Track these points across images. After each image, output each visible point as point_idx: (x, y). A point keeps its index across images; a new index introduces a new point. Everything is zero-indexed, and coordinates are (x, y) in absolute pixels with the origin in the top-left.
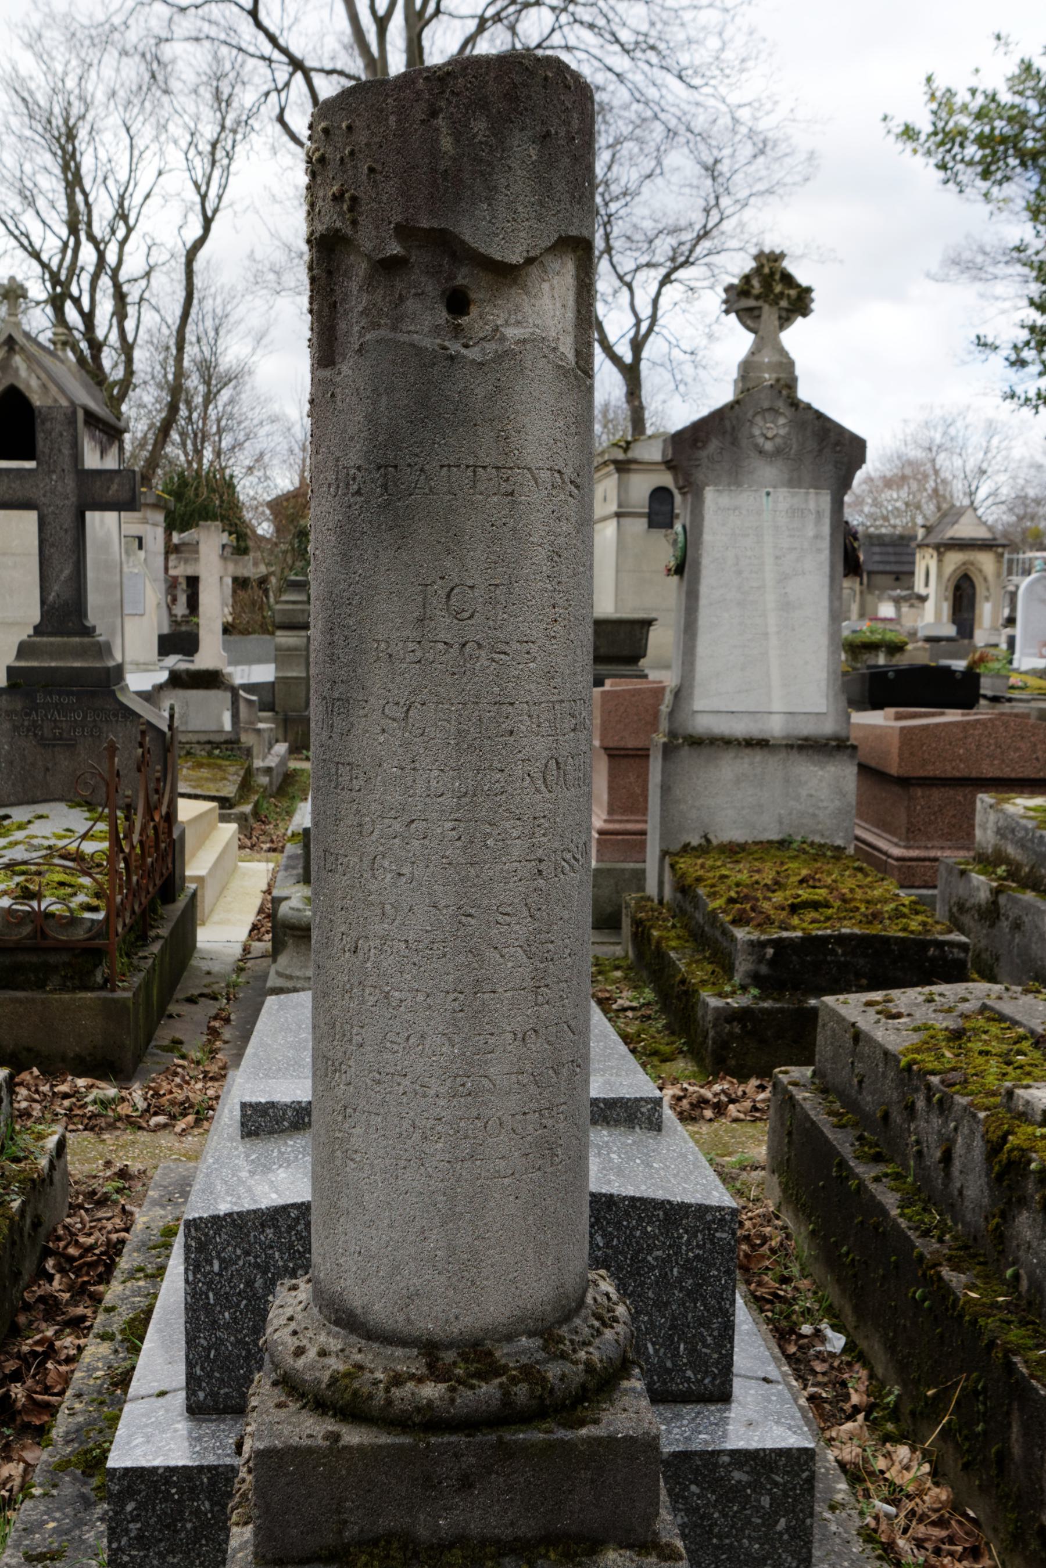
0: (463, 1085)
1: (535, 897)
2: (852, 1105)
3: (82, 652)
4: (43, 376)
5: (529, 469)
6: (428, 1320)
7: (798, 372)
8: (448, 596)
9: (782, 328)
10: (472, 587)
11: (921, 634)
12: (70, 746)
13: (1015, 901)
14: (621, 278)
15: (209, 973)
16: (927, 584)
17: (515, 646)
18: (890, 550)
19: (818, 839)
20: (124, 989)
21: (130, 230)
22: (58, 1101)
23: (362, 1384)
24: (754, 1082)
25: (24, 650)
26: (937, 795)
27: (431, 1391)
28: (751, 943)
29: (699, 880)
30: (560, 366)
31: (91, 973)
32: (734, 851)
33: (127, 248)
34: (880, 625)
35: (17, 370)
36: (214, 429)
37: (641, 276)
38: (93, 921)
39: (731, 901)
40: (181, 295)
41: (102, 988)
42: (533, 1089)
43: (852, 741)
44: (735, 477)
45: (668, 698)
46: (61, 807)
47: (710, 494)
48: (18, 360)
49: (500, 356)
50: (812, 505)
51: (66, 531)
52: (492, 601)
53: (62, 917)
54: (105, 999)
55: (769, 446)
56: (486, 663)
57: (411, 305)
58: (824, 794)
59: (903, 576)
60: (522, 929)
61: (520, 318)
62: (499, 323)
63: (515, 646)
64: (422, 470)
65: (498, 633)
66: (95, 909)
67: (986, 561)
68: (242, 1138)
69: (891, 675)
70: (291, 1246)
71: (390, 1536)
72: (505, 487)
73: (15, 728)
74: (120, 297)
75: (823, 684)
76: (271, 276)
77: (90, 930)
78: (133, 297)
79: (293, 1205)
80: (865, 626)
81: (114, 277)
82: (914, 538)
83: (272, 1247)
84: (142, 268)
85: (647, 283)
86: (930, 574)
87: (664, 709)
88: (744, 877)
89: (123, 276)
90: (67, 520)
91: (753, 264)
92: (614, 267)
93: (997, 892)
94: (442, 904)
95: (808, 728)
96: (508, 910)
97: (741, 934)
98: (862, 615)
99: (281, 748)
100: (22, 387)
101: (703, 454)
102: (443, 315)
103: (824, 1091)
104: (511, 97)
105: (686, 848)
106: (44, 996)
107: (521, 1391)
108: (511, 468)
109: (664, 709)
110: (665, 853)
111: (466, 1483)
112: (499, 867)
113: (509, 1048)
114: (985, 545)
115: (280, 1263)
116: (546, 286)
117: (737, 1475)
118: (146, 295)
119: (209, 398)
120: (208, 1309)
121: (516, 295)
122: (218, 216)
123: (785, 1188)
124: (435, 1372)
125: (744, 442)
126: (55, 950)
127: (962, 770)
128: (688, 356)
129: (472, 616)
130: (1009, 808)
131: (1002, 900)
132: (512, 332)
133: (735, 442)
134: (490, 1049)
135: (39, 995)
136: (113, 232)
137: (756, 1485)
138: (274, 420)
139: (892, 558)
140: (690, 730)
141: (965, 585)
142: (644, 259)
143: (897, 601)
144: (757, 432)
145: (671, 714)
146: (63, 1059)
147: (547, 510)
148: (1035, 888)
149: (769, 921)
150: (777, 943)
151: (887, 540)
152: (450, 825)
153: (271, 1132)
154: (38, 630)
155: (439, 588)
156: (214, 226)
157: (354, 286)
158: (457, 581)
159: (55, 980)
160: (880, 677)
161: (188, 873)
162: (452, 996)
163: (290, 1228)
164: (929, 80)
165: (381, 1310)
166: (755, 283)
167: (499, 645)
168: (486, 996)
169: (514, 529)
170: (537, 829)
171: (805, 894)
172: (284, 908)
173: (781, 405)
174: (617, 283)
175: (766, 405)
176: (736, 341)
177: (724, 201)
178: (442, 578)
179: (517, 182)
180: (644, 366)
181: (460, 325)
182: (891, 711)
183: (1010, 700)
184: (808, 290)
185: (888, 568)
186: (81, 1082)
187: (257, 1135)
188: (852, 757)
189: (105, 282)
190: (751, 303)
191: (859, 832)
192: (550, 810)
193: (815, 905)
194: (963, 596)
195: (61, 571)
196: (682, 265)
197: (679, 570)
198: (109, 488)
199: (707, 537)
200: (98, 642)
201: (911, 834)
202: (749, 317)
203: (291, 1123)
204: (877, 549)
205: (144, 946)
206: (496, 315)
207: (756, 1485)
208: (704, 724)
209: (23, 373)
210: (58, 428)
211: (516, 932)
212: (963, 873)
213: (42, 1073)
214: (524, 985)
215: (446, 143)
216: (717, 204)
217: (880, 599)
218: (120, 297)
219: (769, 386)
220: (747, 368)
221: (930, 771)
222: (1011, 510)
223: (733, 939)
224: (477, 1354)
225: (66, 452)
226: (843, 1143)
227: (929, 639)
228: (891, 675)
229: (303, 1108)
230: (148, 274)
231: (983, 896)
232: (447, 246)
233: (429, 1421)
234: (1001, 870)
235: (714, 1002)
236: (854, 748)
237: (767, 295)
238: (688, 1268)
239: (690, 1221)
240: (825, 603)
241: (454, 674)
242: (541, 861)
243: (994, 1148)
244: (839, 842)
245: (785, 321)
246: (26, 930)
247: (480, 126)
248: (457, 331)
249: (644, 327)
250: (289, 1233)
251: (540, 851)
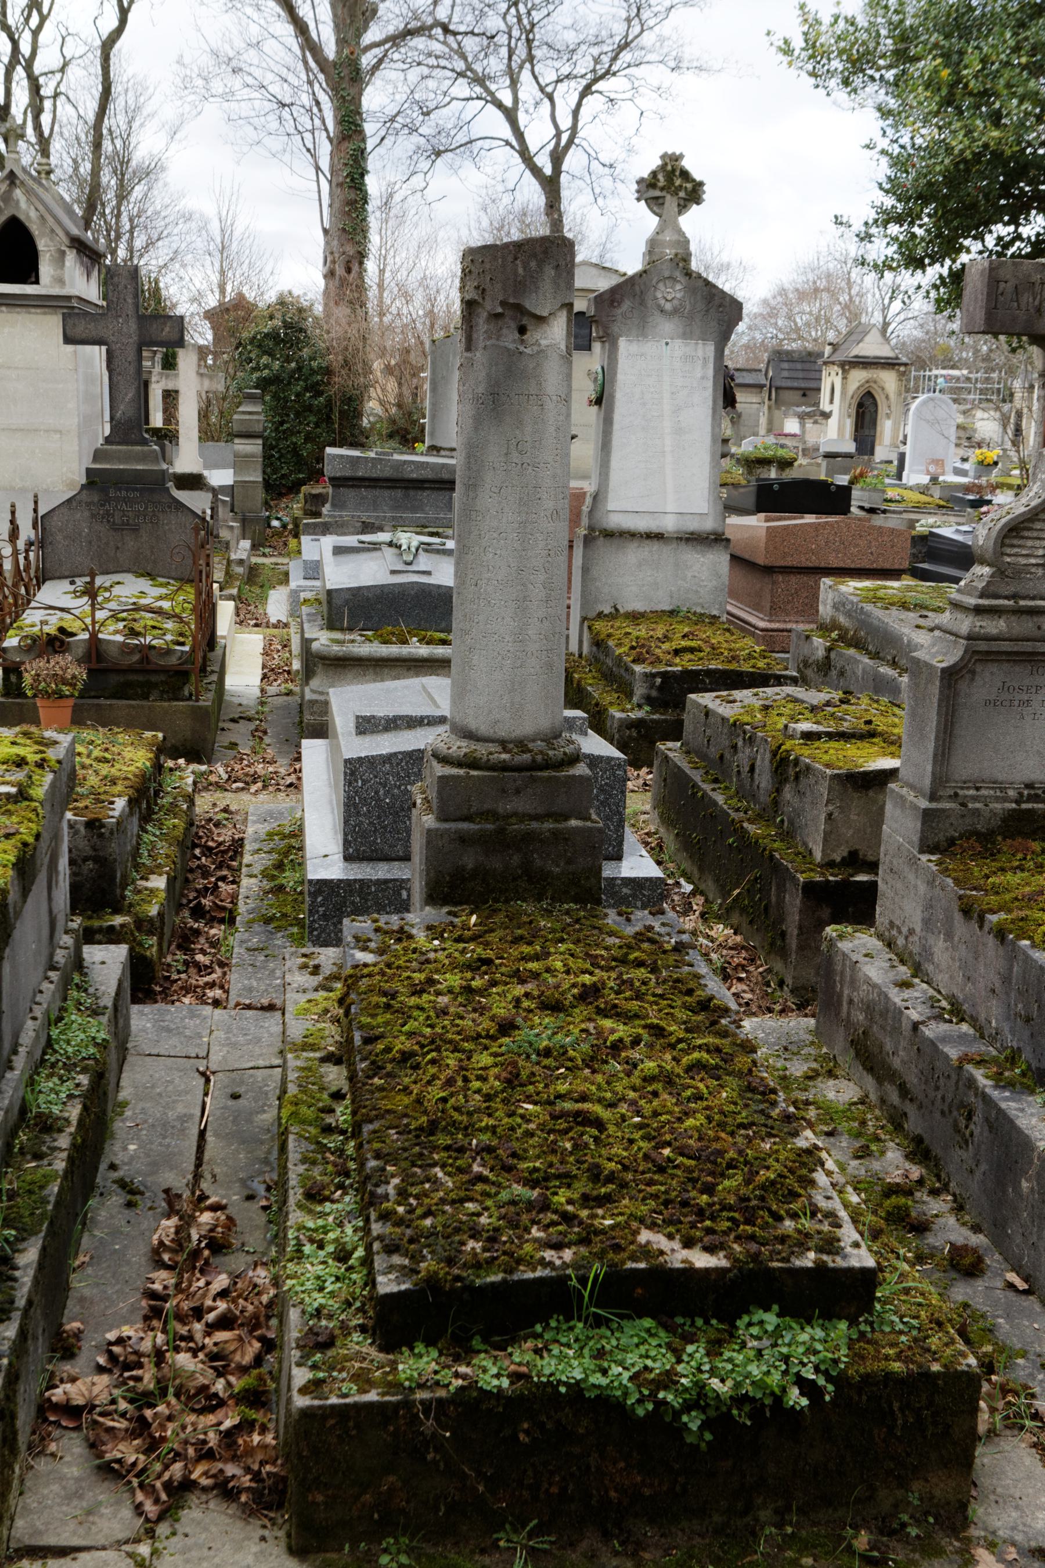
2: (704, 757)
4: (41, 207)
6: (502, 733)
7: (693, 248)
9: (680, 213)
11: (823, 449)
12: (135, 530)
13: (841, 655)
14: (542, 89)
16: (831, 402)
18: (799, 366)
19: (699, 610)
21: (43, 19)
23: (478, 755)
24: (645, 770)
25: (97, 456)
26: (794, 580)
27: (505, 756)
28: (646, 675)
29: (609, 636)
31: (181, 688)
32: (635, 617)
33: (42, 38)
34: (787, 442)
36: (127, 227)
37: (562, 87)
39: (633, 648)
40: (97, 90)
41: (189, 699)
43: (727, 535)
44: (643, 330)
45: (588, 500)
46: (128, 578)
47: (622, 343)
48: (18, 193)
50: (700, 353)
55: (668, 306)
57: (505, 331)
58: (705, 576)
59: (809, 392)
60: (542, 577)
66: (183, 644)
67: (889, 380)
69: (776, 487)
71: (488, 811)
73: (93, 516)
74: (35, 88)
75: (706, 492)
76: (200, 82)
78: (47, 91)
80: (771, 440)
81: (29, 68)
82: (821, 355)
84: (58, 63)
85: (567, 96)
86: (836, 391)
87: (585, 509)
88: (643, 633)
89: (38, 68)
91: (659, 162)
92: (536, 78)
93: (829, 650)
95: (693, 525)
97: (638, 668)
98: (769, 430)
99: (246, 544)
100: (22, 217)
101: (619, 311)
102: (517, 335)
103: (688, 752)
104: (545, 252)
105: (600, 615)
107: (539, 758)
109: (585, 509)
110: (584, 619)
111: (518, 792)
114: (889, 364)
117: (625, 890)
118: (62, 88)
119: (122, 195)
120: (355, 805)
121: (545, 327)
122: (134, 7)
123: (661, 816)
124: (505, 750)
125: (650, 303)
126: (155, 672)
127: (814, 562)
128: (607, 170)
130: (843, 588)
131: (833, 655)
132: (543, 342)
133: (642, 303)
135: (145, 703)
136: (27, 20)
137: (634, 896)
138: (188, 217)
139: (800, 375)
140: (605, 526)
141: (868, 402)
142: (565, 70)
143: (802, 417)
144: (659, 295)
145: (591, 512)
148: (856, 647)
149: (659, 660)
150: (664, 675)
151: (796, 356)
154: (108, 440)
156: (130, 16)
157: (481, 321)
160: (781, 491)
164: (802, 7)
165: (484, 729)
166: (661, 177)
171: (684, 643)
172: (315, 646)
173: (678, 274)
174: (540, 95)
175: (667, 274)
176: (646, 221)
177: (645, 14)
179: (546, 285)
180: (564, 178)
182: (762, 515)
183: (884, 512)
184: (701, 184)
185: (795, 384)
188: (726, 547)
189: (20, 72)
190: (657, 193)
191: (729, 608)
193: (692, 650)
194: (865, 413)
196: (602, 77)
197: (599, 401)
199: (620, 377)
201: (774, 611)
202: (655, 203)
204: (785, 365)
206: (537, 335)
207: (634, 896)
208: (616, 521)
209: (23, 204)
210: (124, 282)
212: (808, 637)
215: (521, 271)
216: (638, 15)
217: (786, 415)
218: (35, 88)
219: (671, 261)
220: (653, 245)
221: (789, 562)
222: (921, 326)
223: (633, 673)
224: (521, 745)
226: (697, 776)
227: (829, 456)
228: (776, 487)
230: (62, 70)
231: (821, 653)
232: (519, 309)
233: (504, 767)
234: (834, 635)
235: (618, 715)
236: (728, 540)
237: (669, 187)
238: (601, 790)
239: (603, 765)
240: (709, 429)
243: (774, 753)
244: (715, 612)
245: (683, 208)
246: (136, 657)
247: (533, 264)
248: (522, 341)
249: (565, 138)
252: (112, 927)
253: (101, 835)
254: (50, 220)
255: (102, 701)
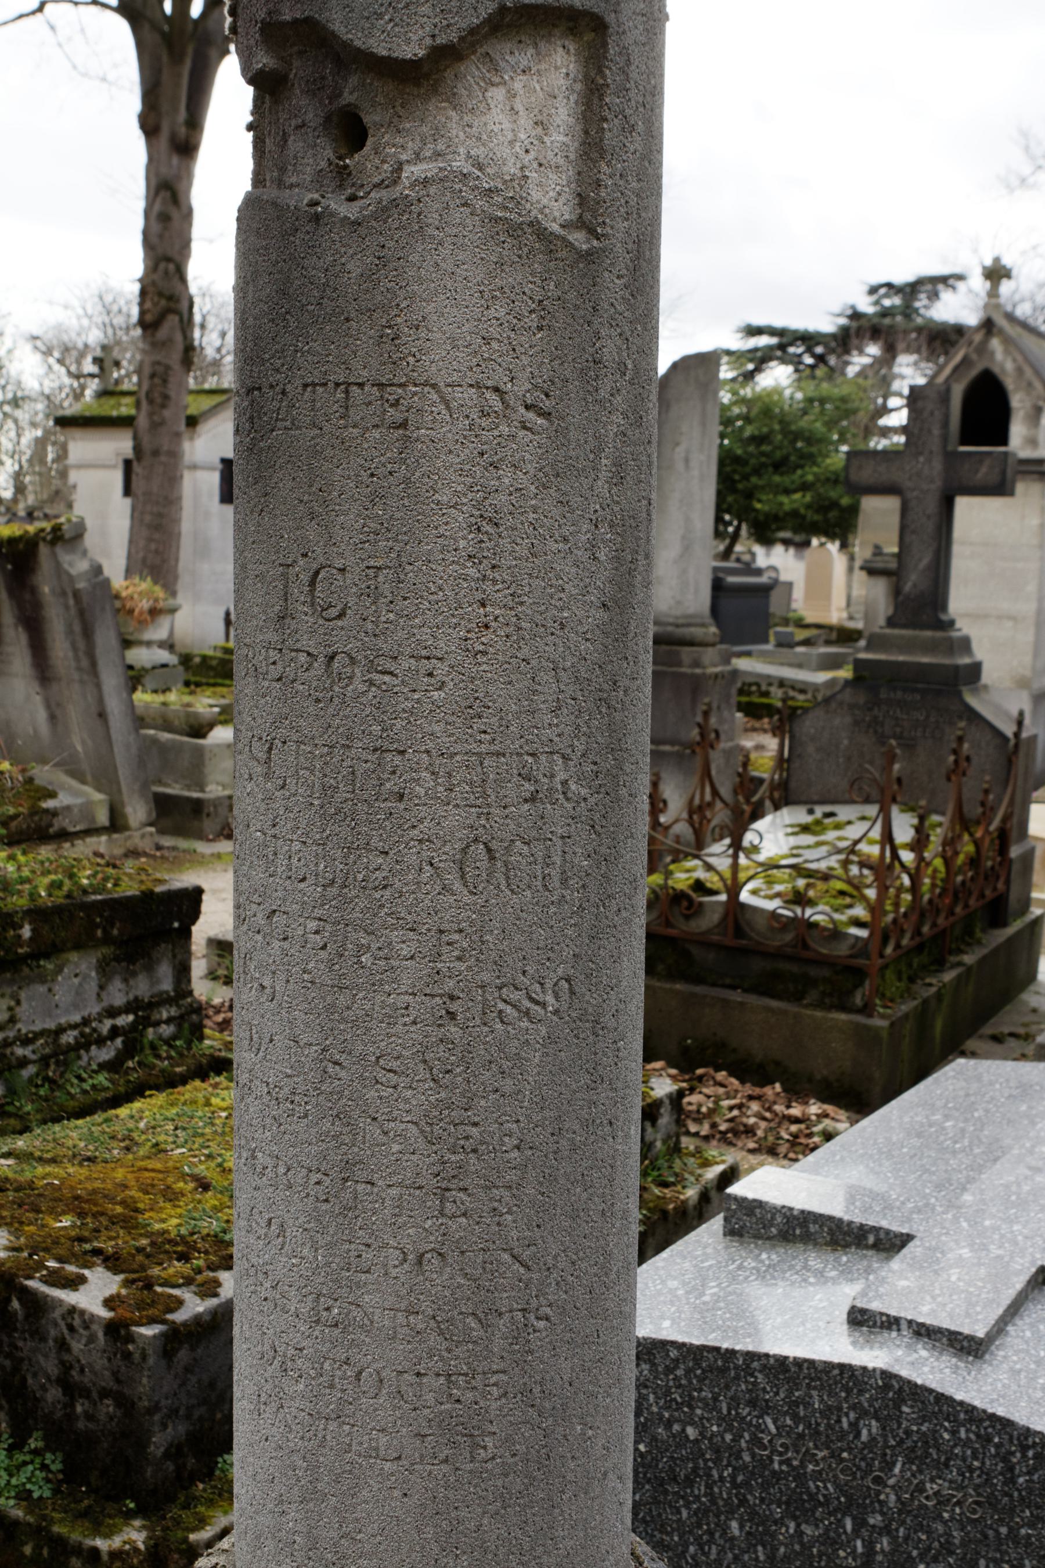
0: (327, 1309)
1: (441, 1051)
3: (931, 647)
4: (1019, 358)
5: (434, 386)
8: (313, 583)
10: (342, 570)
15: (1034, 1011)
17: (406, 663)
20: (883, 1016)
22: (786, 1124)
30: (497, 220)
31: (851, 992)
35: (992, 354)
38: (857, 938)
42: (433, 1339)
49: (385, 209)
51: (929, 517)
52: (373, 594)
53: (825, 929)
54: (858, 1025)
56: (362, 688)
61: (441, 146)
62: (404, 157)
63: (406, 663)
64: (284, 392)
65: (380, 643)
68: (725, 1235)
70: (668, 1393)
72: (393, 414)
73: (856, 723)
77: (853, 947)
79: (673, 1343)
83: (646, 1387)
90: (932, 505)
94: (304, 1039)
96: (394, 1065)
100: (996, 370)
106: (796, 1009)
108: (401, 385)
112: (379, 998)
113: (394, 1272)
115: (655, 1409)
116: (497, 94)
129: (341, 615)
134: (365, 1266)
146: (810, 1080)
147: (471, 449)
152: (312, 925)
153: (757, 1237)
155: (302, 569)
158: (321, 559)
159: (813, 995)
161: (1035, 895)
162: (315, 1177)
163: (669, 1370)
167: (381, 661)
168: (360, 1187)
169: (407, 481)
170: (445, 949)
178: (305, 555)
181: (346, 167)
186: (814, 1109)
187: (741, 1236)
192: (472, 923)
195: (920, 560)
198: (977, 471)
200: (950, 639)
203: (780, 1231)
205: (937, 971)
209: (999, 355)
211: (407, 1101)
213: (785, 1090)
214: (420, 1181)
225: (936, 431)
229: (795, 1218)
241: (318, 701)
242: (452, 998)
246: (789, 937)
248: (342, 175)
250: (667, 1375)
251: (451, 983)
252: (95, 1551)
253: (127, 1356)
254: (1029, 373)
255: (737, 996)
